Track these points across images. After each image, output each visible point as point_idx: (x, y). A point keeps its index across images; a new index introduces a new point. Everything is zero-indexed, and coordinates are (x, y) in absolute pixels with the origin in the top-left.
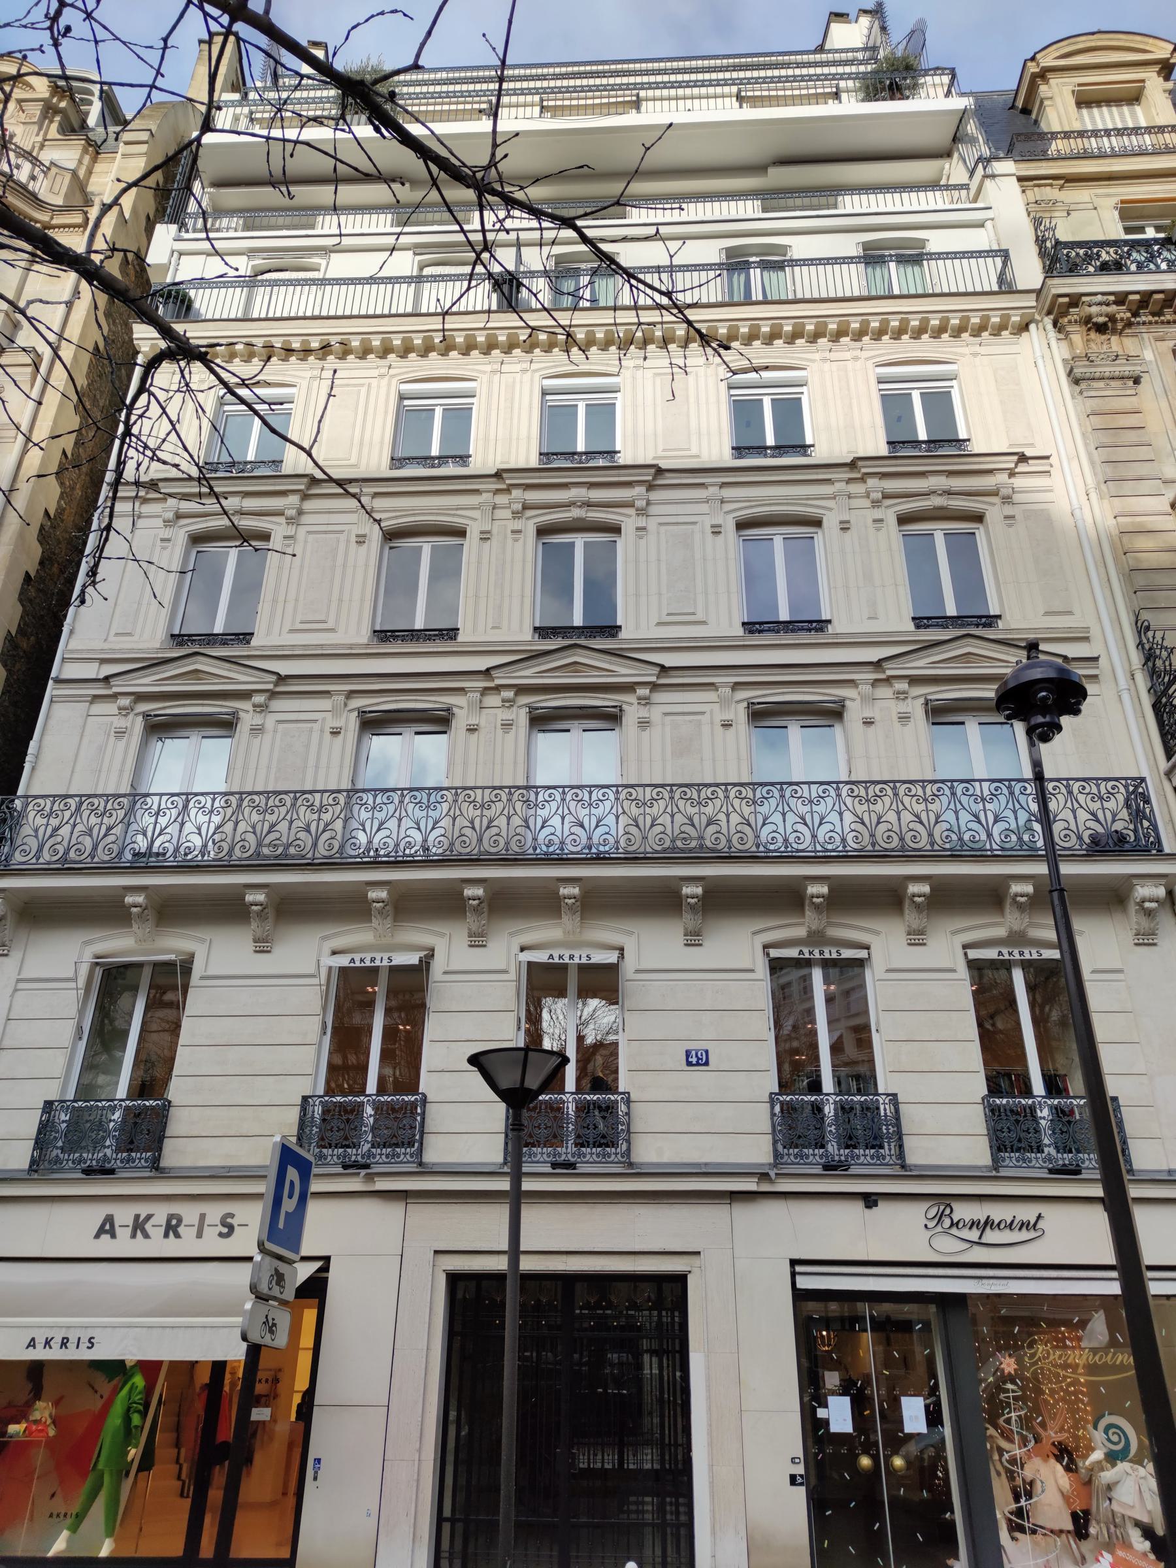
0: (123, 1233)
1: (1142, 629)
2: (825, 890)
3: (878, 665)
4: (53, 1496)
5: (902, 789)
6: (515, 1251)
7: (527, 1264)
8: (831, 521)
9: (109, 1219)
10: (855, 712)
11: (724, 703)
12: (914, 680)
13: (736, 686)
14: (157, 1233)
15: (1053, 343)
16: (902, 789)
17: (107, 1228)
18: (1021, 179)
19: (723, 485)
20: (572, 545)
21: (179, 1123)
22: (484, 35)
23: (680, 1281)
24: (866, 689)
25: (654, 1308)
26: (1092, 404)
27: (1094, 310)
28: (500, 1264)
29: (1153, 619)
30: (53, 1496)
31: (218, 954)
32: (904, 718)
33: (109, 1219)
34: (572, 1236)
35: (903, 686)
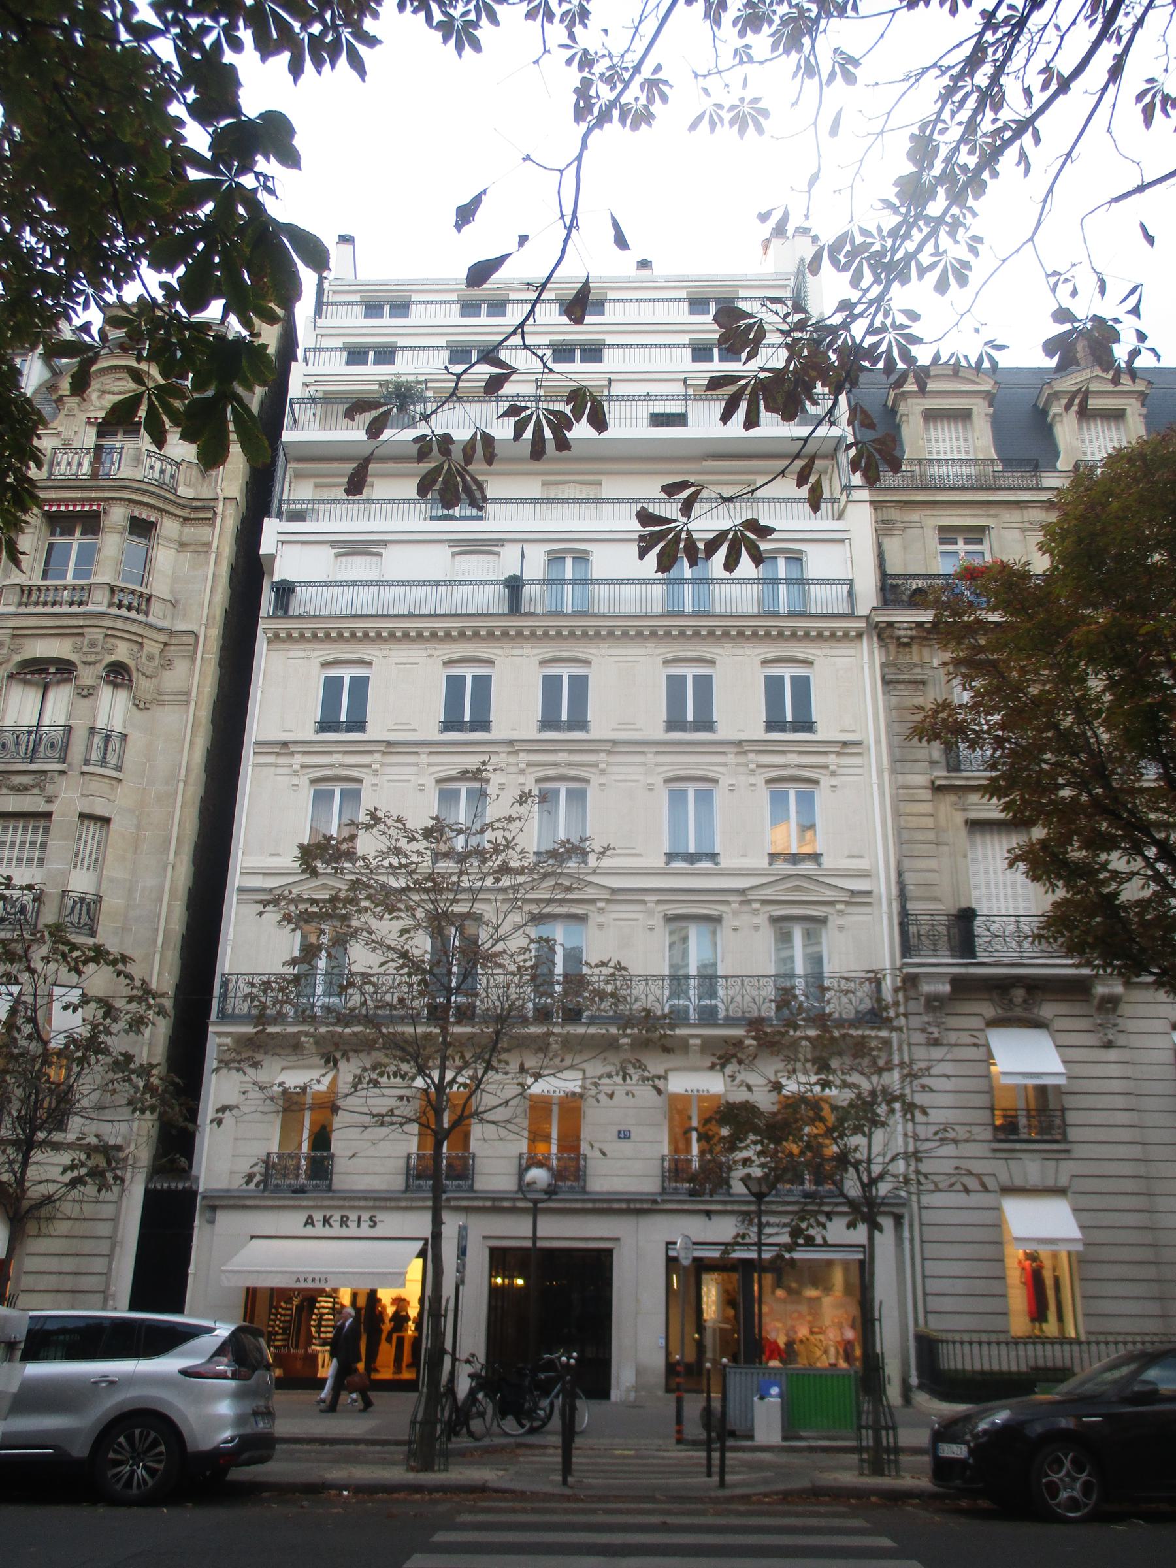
0: (319, 1225)
1: (900, 874)
2: (698, 1042)
3: (743, 892)
4: (604, 1154)
5: (747, 980)
6: (535, 1238)
7: (540, 1244)
8: (725, 781)
9: (310, 1217)
10: (729, 922)
11: (651, 913)
12: (764, 902)
13: (659, 902)
14: (336, 1225)
15: (876, 652)
16: (747, 980)
17: (310, 1222)
18: (871, 502)
19: (657, 753)
20: (558, 791)
21: (341, 1165)
22: (527, 158)
23: (609, 1252)
24: (735, 906)
25: (590, 1272)
26: (894, 701)
27: (902, 633)
28: (529, 1244)
29: (907, 864)
30: (604, 1154)
31: (531, 731)
32: (756, 927)
33: (310, 1217)
34: (561, 1231)
35: (756, 906)
